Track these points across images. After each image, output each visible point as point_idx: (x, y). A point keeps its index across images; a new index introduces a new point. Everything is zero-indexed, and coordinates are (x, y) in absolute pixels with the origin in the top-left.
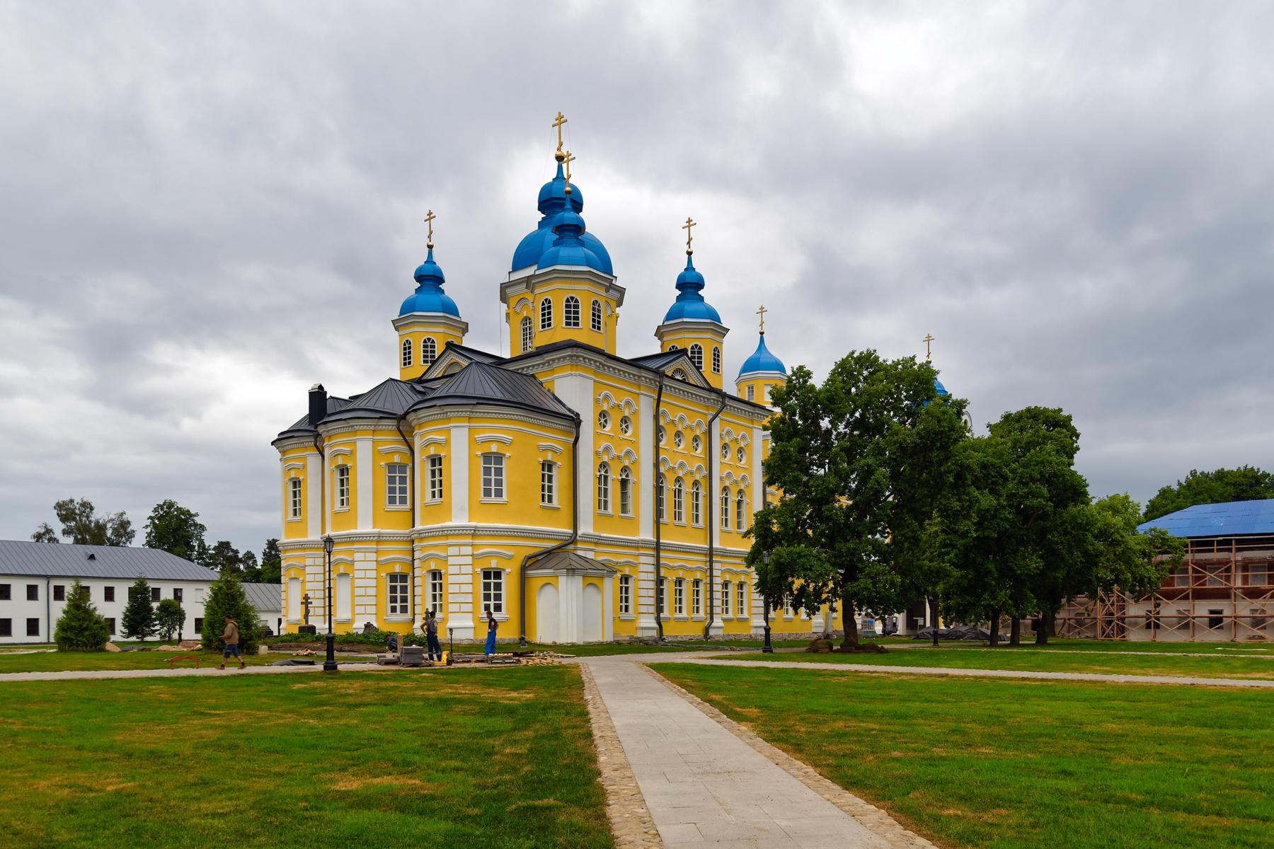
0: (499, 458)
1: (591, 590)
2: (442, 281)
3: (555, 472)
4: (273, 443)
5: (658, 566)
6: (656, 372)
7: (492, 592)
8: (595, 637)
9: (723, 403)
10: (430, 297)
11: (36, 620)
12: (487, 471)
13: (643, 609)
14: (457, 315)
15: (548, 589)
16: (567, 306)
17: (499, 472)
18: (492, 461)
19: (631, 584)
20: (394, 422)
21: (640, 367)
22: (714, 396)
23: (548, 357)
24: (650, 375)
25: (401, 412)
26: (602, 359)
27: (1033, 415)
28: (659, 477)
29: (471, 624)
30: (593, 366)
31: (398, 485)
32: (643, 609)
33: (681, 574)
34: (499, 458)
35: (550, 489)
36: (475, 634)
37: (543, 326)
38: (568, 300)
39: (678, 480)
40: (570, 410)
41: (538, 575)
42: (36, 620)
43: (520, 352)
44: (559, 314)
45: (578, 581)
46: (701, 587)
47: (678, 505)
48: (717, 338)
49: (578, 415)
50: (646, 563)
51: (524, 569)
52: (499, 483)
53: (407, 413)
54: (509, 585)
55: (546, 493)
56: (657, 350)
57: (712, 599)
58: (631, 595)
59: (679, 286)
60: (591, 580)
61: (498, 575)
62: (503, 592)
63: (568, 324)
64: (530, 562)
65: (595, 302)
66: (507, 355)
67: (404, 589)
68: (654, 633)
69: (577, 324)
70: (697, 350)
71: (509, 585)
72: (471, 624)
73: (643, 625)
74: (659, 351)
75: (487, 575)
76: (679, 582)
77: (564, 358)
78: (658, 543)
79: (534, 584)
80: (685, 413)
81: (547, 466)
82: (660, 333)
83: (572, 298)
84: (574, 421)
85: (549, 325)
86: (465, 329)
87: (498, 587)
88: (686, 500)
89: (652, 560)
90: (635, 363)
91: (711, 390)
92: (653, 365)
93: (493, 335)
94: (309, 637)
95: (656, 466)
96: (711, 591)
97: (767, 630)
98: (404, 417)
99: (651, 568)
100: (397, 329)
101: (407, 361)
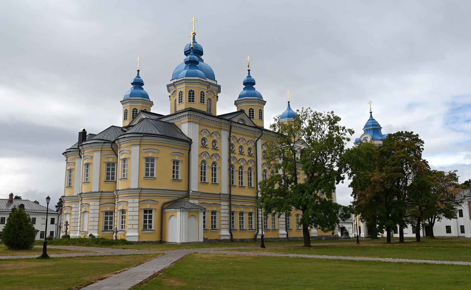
0: (153, 159)
1: (193, 219)
2: (143, 84)
3: (180, 165)
4: (63, 154)
5: (230, 206)
6: (228, 120)
7: (148, 219)
8: (194, 239)
9: (262, 133)
10: (138, 91)
11: (51, 224)
12: (147, 165)
13: (223, 226)
14: (148, 98)
15: (173, 218)
16: (189, 94)
17: (152, 165)
18: (149, 161)
19: (217, 215)
20: (110, 144)
21: (221, 119)
22: (257, 130)
23: (178, 115)
24: (226, 122)
25: (113, 140)
26: (203, 116)
27: (409, 135)
28: (231, 166)
29: (137, 234)
30: (198, 119)
31: (150, 168)
32: (223, 226)
33: (242, 210)
34: (153, 159)
35: (177, 172)
36: (139, 239)
37: (179, 102)
38: (189, 91)
39: (241, 167)
40: (188, 138)
41: (169, 212)
42: (51, 224)
43: (173, 112)
44: (185, 97)
45: (185, 214)
46: (253, 216)
47: (241, 178)
48: (261, 106)
49: (191, 140)
50: (224, 205)
51: (162, 210)
52: (152, 170)
53: (115, 141)
54: (155, 216)
55: (175, 174)
56: (235, 110)
57: (258, 221)
58: (217, 220)
59: (244, 84)
60: (193, 214)
61: (151, 211)
62: (153, 219)
63: (189, 101)
64: (165, 206)
65: (202, 92)
66: (165, 114)
67: (111, 218)
68: (285, 236)
69: (193, 101)
70: (251, 111)
71: (155, 216)
72: (137, 234)
73: (222, 234)
74: (236, 111)
75: (145, 211)
76: (241, 214)
77: (185, 115)
78: (230, 195)
79: (168, 215)
80: (243, 139)
81: (176, 162)
82: (236, 103)
83: (192, 90)
84: (189, 142)
85: (182, 102)
86: (151, 104)
87: (151, 217)
88: (245, 176)
89: (227, 204)
90: (221, 117)
91: (256, 127)
92: (227, 118)
93: (162, 107)
94: (66, 239)
95: (229, 161)
96: (258, 218)
97: (287, 235)
98: (114, 142)
99: (227, 207)
100: (122, 104)
101: (125, 118)
